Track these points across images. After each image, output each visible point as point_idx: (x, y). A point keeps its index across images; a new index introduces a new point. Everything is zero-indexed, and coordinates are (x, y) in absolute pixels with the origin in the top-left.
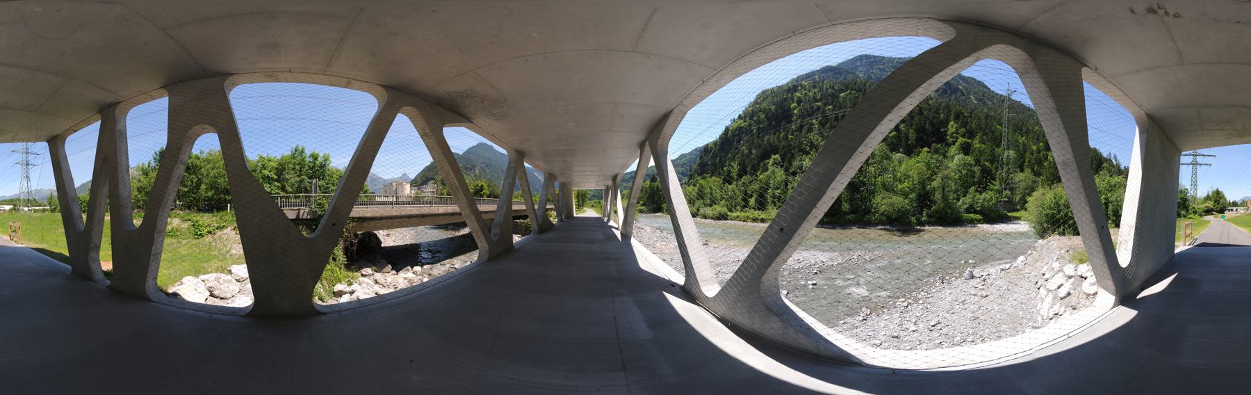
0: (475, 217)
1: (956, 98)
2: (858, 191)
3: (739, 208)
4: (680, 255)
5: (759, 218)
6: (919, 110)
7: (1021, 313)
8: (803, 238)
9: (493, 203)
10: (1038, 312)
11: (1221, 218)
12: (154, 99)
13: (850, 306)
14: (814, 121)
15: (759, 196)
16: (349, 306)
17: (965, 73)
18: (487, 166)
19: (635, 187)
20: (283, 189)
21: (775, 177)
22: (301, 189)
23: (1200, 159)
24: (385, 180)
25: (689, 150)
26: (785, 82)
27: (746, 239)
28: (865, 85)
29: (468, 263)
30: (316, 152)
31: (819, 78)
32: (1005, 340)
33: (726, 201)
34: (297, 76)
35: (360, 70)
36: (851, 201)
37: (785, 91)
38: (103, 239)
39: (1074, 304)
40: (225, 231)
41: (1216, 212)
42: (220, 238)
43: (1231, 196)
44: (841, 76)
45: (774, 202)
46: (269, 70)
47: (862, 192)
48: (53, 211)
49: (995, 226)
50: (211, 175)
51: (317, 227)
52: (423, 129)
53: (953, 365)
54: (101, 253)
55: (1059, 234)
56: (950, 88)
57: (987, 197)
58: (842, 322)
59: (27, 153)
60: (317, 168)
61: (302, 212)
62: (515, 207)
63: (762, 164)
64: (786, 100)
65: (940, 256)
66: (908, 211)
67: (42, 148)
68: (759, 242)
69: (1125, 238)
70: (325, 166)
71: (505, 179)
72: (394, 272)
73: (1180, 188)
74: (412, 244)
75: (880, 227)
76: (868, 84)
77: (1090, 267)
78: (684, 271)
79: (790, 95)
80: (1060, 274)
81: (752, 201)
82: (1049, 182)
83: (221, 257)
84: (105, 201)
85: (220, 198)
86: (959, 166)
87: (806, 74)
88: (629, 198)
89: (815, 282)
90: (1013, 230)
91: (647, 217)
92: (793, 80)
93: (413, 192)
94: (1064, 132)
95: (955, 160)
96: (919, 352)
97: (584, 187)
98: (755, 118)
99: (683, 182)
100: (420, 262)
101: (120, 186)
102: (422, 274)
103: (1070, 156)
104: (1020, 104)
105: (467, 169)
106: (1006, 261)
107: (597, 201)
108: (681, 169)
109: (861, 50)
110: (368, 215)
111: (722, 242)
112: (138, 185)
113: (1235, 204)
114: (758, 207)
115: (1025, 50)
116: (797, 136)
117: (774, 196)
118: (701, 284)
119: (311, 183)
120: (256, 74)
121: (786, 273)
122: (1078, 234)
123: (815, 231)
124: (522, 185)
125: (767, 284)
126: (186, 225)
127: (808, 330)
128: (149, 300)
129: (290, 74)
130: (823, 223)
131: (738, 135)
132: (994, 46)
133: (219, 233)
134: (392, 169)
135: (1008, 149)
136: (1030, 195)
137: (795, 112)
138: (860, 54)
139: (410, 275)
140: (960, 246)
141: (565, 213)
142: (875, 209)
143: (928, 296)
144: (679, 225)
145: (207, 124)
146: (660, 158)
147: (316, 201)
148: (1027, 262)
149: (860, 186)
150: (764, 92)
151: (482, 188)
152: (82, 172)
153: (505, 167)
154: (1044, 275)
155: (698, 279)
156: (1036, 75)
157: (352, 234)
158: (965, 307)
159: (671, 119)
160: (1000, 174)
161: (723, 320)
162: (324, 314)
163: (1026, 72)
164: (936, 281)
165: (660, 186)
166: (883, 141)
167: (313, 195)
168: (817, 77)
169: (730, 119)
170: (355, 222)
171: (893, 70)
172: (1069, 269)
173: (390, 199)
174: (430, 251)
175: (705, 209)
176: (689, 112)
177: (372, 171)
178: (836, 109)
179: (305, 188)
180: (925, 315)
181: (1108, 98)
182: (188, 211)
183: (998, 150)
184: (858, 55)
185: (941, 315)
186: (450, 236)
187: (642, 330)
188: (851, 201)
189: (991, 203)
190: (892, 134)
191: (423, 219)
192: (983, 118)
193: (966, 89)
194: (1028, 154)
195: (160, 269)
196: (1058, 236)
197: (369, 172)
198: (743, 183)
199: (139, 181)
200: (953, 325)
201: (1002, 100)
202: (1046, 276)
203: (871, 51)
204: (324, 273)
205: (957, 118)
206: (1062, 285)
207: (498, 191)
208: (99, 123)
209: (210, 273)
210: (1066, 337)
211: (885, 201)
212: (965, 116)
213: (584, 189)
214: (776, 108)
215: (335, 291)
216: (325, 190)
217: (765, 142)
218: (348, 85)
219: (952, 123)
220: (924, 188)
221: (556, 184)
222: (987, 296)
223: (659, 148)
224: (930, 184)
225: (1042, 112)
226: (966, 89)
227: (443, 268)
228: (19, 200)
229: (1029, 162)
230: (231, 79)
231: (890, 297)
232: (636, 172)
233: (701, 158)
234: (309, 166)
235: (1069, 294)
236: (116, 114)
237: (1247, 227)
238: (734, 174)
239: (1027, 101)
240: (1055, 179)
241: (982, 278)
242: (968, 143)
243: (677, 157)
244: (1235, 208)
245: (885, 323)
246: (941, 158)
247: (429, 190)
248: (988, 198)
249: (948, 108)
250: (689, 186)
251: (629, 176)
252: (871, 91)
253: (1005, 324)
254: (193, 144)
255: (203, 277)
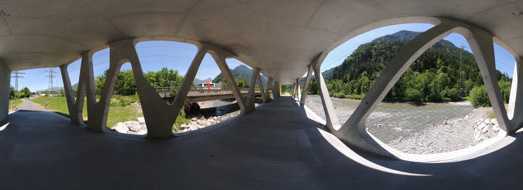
1: (441, 49)
2: (399, 87)
3: (350, 93)
4: (324, 113)
6: (425, 54)
7: (467, 139)
8: (376, 106)
9: (247, 90)
12: (104, 49)
13: (395, 135)
14: (381, 58)
17: (445, 39)
18: (244, 74)
19: (306, 84)
20: (159, 85)
21: (365, 81)
22: (166, 85)
26: (370, 41)
27: (352, 107)
28: (403, 43)
29: (236, 115)
30: (172, 69)
31: (384, 40)
32: (460, 150)
33: (344, 90)
34: (163, 38)
36: (396, 91)
38: (84, 108)
39: (489, 135)
40: (135, 103)
41: (26, 97)
42: (133, 106)
44: (393, 39)
45: (364, 91)
46: (151, 36)
48: (63, 96)
49: (456, 103)
50: (129, 80)
51: (173, 101)
52: (217, 59)
53: (438, 161)
54: (83, 114)
56: (438, 45)
57: (453, 91)
58: (391, 142)
59: (52, 72)
60: (173, 76)
61: (167, 94)
62: (256, 92)
64: (370, 49)
66: (419, 96)
67: (58, 70)
68: (358, 108)
70: (176, 75)
71: (252, 80)
72: (205, 119)
75: (408, 103)
77: (496, 120)
78: (326, 119)
80: (484, 123)
81: (355, 91)
83: (133, 114)
84: (84, 91)
85: (133, 89)
87: (379, 38)
88: (304, 88)
89: (380, 125)
90: (464, 105)
91: (311, 97)
92: (373, 40)
94: (485, 64)
96: (423, 155)
98: (357, 56)
99: (326, 82)
101: (91, 85)
102: (217, 120)
103: (488, 74)
104: (467, 52)
105: (236, 76)
108: (325, 77)
110: (195, 95)
112: (98, 84)
116: (374, 64)
117: (364, 89)
118: (333, 124)
119: (170, 82)
120: (146, 37)
121: (368, 121)
123: (381, 104)
124: (259, 82)
125: (360, 125)
126: (118, 101)
127: (377, 145)
128: (104, 133)
129: (160, 37)
130: (384, 101)
131: (350, 63)
132: (457, 28)
133: (132, 104)
135: (462, 71)
136: (471, 90)
137: (374, 54)
138: (402, 30)
139: (212, 120)
140: (442, 111)
141: (277, 95)
142: (406, 95)
143: (428, 131)
144: (324, 100)
145: (126, 59)
146: (317, 72)
147: (172, 90)
148: (469, 118)
149: (400, 85)
150: (361, 45)
151: (242, 84)
152: (74, 79)
153: (252, 75)
154: (476, 123)
155: (332, 122)
157: (188, 104)
158: (443, 136)
159: (322, 56)
160: (459, 81)
162: (177, 137)
163: (470, 38)
165: (316, 84)
166: (410, 67)
167: (171, 87)
168: (383, 39)
170: (189, 98)
171: (415, 37)
172: (487, 121)
174: (220, 110)
175: (335, 93)
178: (391, 53)
179: (168, 84)
180: (426, 139)
181: (504, 49)
182: (119, 95)
183: (458, 71)
185: (433, 139)
186: (229, 104)
187: (308, 143)
189: (455, 93)
191: (217, 97)
194: (470, 73)
195: (108, 120)
196: (482, 107)
197: (195, 77)
199: (98, 83)
200: (438, 144)
201: (460, 50)
204: (177, 120)
205: (441, 58)
206: (484, 127)
207: (249, 85)
208: (81, 59)
209: (129, 121)
210: (486, 149)
211: (411, 92)
212: (444, 57)
214: (366, 52)
215: (181, 127)
216: (176, 85)
218: (185, 41)
219: (439, 60)
220: (427, 86)
221: (273, 82)
222: (452, 132)
223: (316, 68)
224: (429, 85)
226: (445, 46)
227: (226, 117)
228: (48, 91)
229: (470, 76)
230: (136, 39)
231: (411, 132)
232: (307, 77)
233: (334, 72)
234: (169, 75)
235: (487, 131)
236: (88, 55)
238: (348, 79)
239: (470, 51)
240: (481, 83)
241: (451, 125)
242: (445, 68)
245: (409, 143)
246: (434, 74)
248: (453, 91)
249: (437, 53)
250: (329, 84)
251: (303, 79)
252: (406, 46)
253: (460, 144)
254: (121, 67)
255: (126, 122)
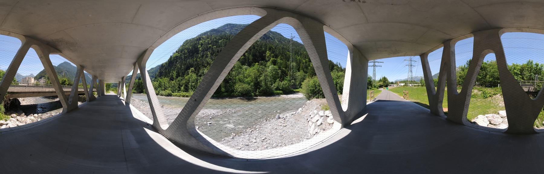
0: (62, 94)
1: (269, 41)
3: (177, 91)
5: (186, 95)
6: (253, 47)
7: (301, 133)
9: (70, 88)
10: (309, 132)
11: (387, 89)
14: (208, 53)
15: (185, 86)
16: (5, 130)
17: (272, 30)
23: (376, 64)
24: (23, 76)
25: (155, 66)
26: (195, 36)
27: (180, 104)
28: (229, 37)
29: (58, 113)
31: (210, 34)
33: (171, 88)
35: (14, 28)
36: (225, 87)
37: (195, 40)
39: (324, 128)
41: (384, 86)
43: (390, 80)
47: (230, 83)
49: (288, 95)
55: (316, 98)
56: (266, 37)
57: (284, 83)
62: (79, 90)
63: (186, 72)
64: (196, 44)
65: (265, 109)
66: (250, 91)
69: (345, 99)
71: (75, 78)
72: (25, 116)
73: (368, 77)
74: (34, 104)
75: (238, 98)
76: (231, 36)
78: (153, 119)
79: (198, 42)
81: (182, 88)
82: (311, 76)
86: (271, 70)
87: (204, 33)
89: (210, 123)
90: (296, 97)
92: (199, 35)
93: (35, 82)
94: (317, 54)
95: (270, 68)
97: (110, 82)
98: (183, 52)
99: (152, 80)
100: (37, 112)
102: (38, 117)
103: (320, 64)
104: (297, 43)
105: (59, 73)
106: (294, 110)
107: (115, 88)
108: (151, 75)
109: (227, 21)
110: (15, 91)
111: (169, 106)
113: (392, 83)
114: (185, 91)
115: (298, 19)
117: (192, 86)
118: (160, 124)
121: (198, 119)
122: (324, 98)
123: (210, 100)
124: (82, 80)
130: (213, 97)
131: (176, 60)
132: (284, 18)
134: (27, 72)
135: (293, 62)
136: (303, 81)
137: (200, 49)
138: (227, 23)
139: (32, 118)
141: (101, 93)
142: (236, 90)
146: (143, 70)
149: (229, 80)
150: (186, 41)
153: (75, 73)
154: (310, 116)
156: (303, 30)
158: (277, 131)
159: (147, 53)
160: (290, 73)
161: (170, 140)
163: (299, 28)
164: (264, 120)
165: (142, 82)
168: (209, 34)
169: (172, 53)
172: (321, 113)
173: (25, 85)
174: (41, 108)
176: (155, 50)
177: (17, 72)
180: (259, 135)
183: (288, 63)
184: (226, 24)
185: (266, 135)
187: (134, 144)
188: (225, 87)
190: (242, 58)
191: (39, 94)
192: (281, 49)
193: (273, 37)
194: (301, 64)
196: (316, 99)
197: (16, 72)
198: (178, 80)
200: (272, 139)
201: (289, 41)
202: (311, 116)
203: (231, 22)
205: (270, 49)
206: (318, 120)
207: (72, 83)
210: (321, 142)
211: (240, 87)
212: (273, 49)
213: (109, 83)
217: (188, 62)
218: (9, 35)
219: (268, 52)
220: (257, 80)
221: (97, 80)
222: (286, 126)
223: (142, 65)
224: (259, 79)
225: (307, 46)
226: (273, 37)
227: (47, 115)
229: (302, 67)
231: (244, 128)
232: (132, 76)
233: (160, 69)
235: (322, 124)
237: (397, 93)
238: (174, 76)
239: (300, 41)
240: (314, 74)
242: (275, 60)
243: (150, 69)
244: (392, 85)
245: (242, 139)
246: (263, 67)
247: (42, 81)
250: (155, 82)
251: (129, 77)
